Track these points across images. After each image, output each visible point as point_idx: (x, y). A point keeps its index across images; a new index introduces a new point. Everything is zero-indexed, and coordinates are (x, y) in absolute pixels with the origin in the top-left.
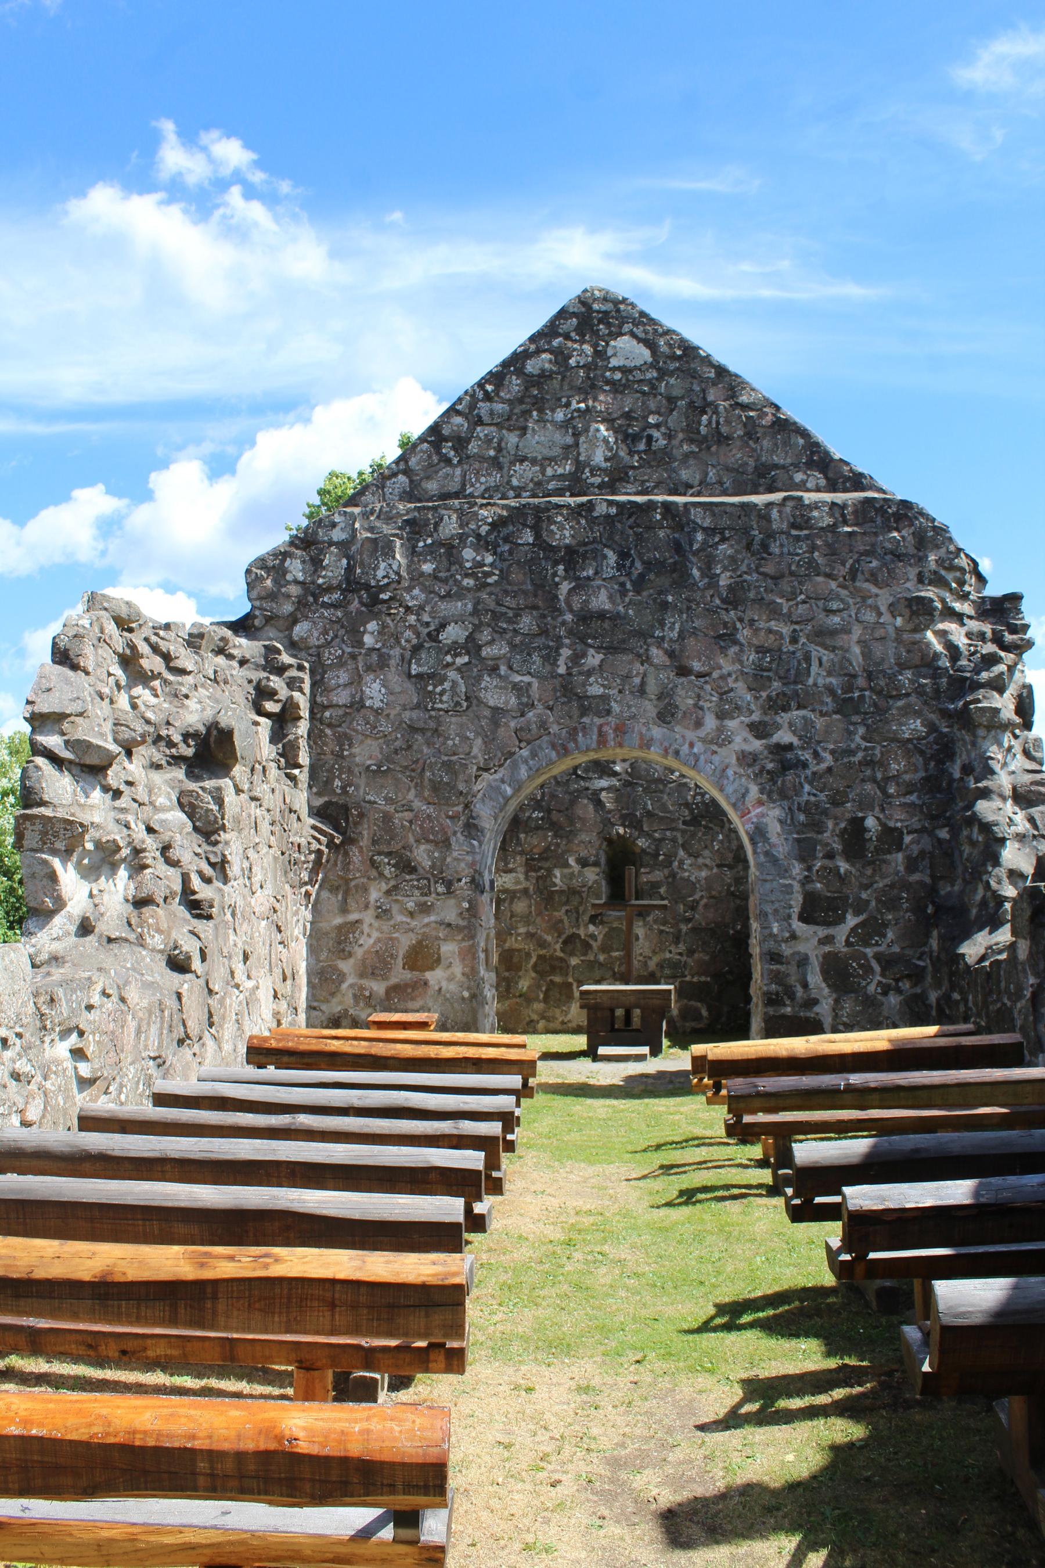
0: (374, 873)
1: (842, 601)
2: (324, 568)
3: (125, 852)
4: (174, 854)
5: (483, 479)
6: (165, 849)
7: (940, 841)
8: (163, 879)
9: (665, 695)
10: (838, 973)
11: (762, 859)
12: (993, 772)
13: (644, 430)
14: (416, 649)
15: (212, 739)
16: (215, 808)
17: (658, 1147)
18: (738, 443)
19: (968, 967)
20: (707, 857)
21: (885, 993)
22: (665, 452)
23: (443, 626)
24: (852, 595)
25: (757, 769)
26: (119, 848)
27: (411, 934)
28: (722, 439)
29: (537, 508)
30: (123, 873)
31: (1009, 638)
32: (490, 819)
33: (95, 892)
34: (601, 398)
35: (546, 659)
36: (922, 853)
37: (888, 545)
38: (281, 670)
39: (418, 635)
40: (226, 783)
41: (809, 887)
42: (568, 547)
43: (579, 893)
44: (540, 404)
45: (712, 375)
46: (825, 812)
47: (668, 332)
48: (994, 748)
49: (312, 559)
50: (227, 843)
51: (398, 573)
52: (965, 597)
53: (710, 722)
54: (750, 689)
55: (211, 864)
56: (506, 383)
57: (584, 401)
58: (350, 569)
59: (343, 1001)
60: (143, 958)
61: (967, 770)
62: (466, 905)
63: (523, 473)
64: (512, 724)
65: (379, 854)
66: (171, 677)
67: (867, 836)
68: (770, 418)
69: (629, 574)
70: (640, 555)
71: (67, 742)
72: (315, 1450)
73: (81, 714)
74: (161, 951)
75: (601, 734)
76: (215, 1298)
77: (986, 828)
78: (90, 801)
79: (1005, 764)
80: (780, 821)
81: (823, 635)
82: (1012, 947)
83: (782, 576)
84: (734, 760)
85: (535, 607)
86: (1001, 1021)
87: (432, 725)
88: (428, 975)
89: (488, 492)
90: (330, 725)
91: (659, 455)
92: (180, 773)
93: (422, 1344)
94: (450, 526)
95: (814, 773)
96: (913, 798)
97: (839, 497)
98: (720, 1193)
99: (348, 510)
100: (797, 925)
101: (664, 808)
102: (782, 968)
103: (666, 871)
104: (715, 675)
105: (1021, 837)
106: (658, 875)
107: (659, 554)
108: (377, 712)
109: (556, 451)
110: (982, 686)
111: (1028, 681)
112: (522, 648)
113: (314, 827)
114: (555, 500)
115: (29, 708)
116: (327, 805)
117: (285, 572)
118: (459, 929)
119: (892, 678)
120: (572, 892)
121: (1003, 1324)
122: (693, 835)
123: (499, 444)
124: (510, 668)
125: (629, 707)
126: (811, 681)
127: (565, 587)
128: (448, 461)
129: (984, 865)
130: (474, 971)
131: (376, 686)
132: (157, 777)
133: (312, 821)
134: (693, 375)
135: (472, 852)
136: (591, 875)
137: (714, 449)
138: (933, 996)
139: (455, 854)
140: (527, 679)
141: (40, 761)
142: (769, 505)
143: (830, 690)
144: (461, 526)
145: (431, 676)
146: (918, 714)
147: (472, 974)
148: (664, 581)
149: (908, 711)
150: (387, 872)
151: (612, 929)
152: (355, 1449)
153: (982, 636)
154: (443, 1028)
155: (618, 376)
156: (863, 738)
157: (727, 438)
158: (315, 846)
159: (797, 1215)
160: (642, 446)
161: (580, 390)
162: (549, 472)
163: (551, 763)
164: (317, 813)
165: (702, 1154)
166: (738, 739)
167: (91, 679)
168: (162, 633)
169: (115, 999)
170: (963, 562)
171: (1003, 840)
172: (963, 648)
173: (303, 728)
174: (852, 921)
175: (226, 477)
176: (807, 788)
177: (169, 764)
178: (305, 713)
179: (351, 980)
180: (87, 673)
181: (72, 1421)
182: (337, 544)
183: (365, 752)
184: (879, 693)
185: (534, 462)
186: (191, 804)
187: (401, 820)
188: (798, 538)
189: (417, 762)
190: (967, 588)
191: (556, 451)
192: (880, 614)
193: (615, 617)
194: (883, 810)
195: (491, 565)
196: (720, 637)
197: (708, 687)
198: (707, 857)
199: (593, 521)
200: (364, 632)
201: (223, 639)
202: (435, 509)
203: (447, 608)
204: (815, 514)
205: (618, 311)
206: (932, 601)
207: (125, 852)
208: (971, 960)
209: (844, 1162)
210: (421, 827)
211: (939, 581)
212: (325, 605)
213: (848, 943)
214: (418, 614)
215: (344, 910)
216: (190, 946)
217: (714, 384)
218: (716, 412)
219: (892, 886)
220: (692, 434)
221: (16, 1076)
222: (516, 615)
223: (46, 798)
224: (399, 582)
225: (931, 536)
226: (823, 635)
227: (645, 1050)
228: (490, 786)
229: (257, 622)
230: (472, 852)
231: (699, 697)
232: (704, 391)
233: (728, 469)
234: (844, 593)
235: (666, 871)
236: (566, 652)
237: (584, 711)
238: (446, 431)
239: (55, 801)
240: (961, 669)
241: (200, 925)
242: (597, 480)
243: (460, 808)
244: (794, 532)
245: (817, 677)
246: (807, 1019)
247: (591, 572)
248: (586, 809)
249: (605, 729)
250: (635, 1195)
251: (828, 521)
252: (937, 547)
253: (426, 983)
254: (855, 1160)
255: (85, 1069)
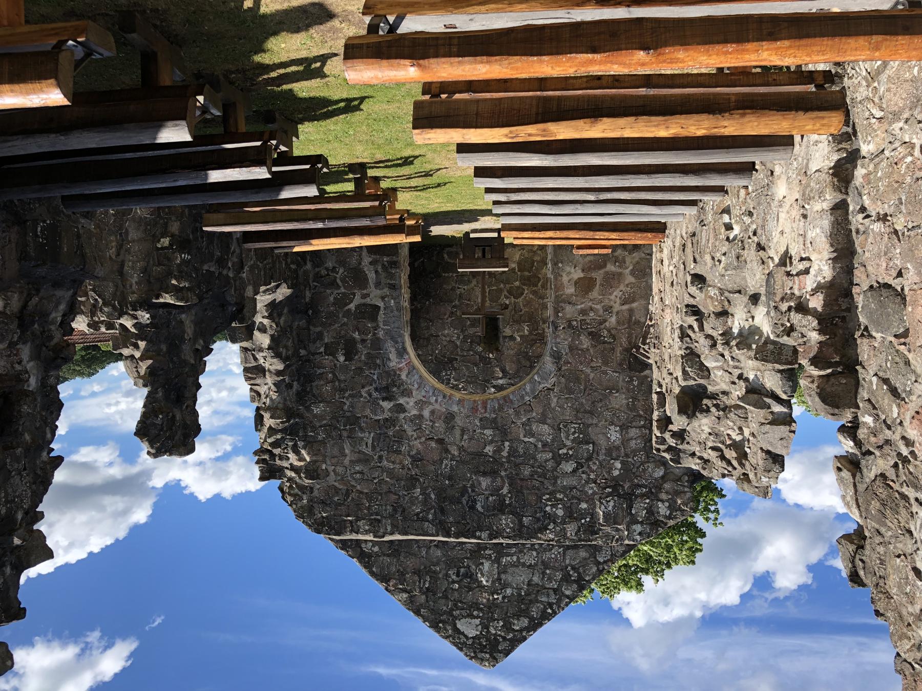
0: (613, 332)
1: (354, 479)
2: (645, 508)
3: (733, 343)
4: (708, 342)
5: (553, 556)
6: (714, 346)
7: (305, 348)
8: (713, 327)
9: (450, 429)
10: (359, 279)
11: (399, 340)
12: (274, 384)
13: (461, 580)
14: (589, 459)
15: (691, 408)
16: (687, 369)
17: (439, 185)
18: (409, 570)
19: (285, 282)
20: (444, 340)
21: (334, 268)
22: (449, 567)
23: (574, 471)
24: (349, 481)
25: (402, 388)
26: (736, 345)
27: (591, 297)
28: (417, 572)
29: (521, 538)
30: (736, 331)
31: (266, 457)
32: (548, 363)
33: (750, 320)
34: (485, 601)
35: (516, 451)
36: (314, 343)
37: (328, 509)
38: (670, 449)
39: (589, 467)
40: (683, 384)
41: (374, 325)
42: (504, 514)
43: (514, 321)
44: (520, 599)
45: (422, 610)
46: (366, 364)
47: (446, 638)
48: (274, 397)
49: (653, 514)
50: (680, 348)
51: (601, 503)
52: (290, 479)
53: (426, 413)
54: (405, 431)
55: (690, 337)
56: (540, 613)
57: (495, 599)
58: (630, 507)
59: (631, 260)
60: (719, 282)
61: (289, 386)
62: (560, 314)
63: (530, 558)
64: (534, 414)
65: (610, 343)
66: (720, 445)
67: (343, 351)
68: (391, 584)
69: (470, 497)
70: (463, 507)
71: (769, 407)
72: (403, 62)
73: (763, 424)
74: (710, 286)
75: (485, 408)
76: (537, 114)
77: (277, 355)
78: (754, 373)
79: (269, 389)
80: (390, 360)
81: (365, 460)
82: (257, 293)
83: (386, 493)
84: (414, 393)
85: (522, 480)
86: (263, 254)
87: (580, 415)
88: (582, 275)
89: (550, 548)
90: (641, 416)
91: (453, 565)
92: (710, 389)
93: (444, 96)
94: (571, 529)
95: (371, 385)
96: (319, 371)
97: (354, 537)
98: (389, 164)
99: (632, 543)
100: (381, 304)
101: (468, 368)
102: (389, 281)
103: (466, 333)
104: (423, 439)
105: (261, 350)
106: (471, 331)
107: (453, 507)
108: (612, 423)
109: (510, 570)
110: (280, 431)
111: (258, 433)
112: (530, 457)
113: (648, 358)
114: (511, 542)
115: (793, 429)
116: (642, 370)
117: (669, 507)
118: (564, 301)
119: (329, 436)
120: (518, 322)
121: (159, 122)
122: (452, 353)
123: (544, 577)
124: (536, 446)
125: (470, 422)
126: (372, 435)
127: (505, 491)
128: (573, 568)
129: (279, 336)
130: (556, 279)
131: (613, 438)
132: (724, 387)
133: (650, 361)
134: (432, 611)
135: (557, 344)
136: (507, 331)
137: (422, 567)
138: (309, 266)
139: (566, 342)
140: (526, 439)
141: (784, 397)
142: (392, 534)
143: (362, 430)
144: (565, 529)
145: (581, 443)
146: (315, 416)
147: (557, 275)
148: (450, 492)
149: (320, 417)
150: (606, 332)
151: (496, 301)
152: (385, 62)
153: (281, 458)
154: (572, 246)
155: (475, 613)
156: (345, 404)
157: (415, 573)
158: (646, 347)
159: (320, 158)
160: (462, 570)
161: (497, 606)
162: (515, 558)
163: (513, 393)
164: (648, 366)
165: (413, 183)
166: (411, 404)
167: (759, 445)
168: (726, 472)
169: (716, 259)
170: (289, 499)
171: (268, 349)
172: (290, 451)
173: (656, 415)
174: (352, 306)
175: (758, 575)
176: (375, 377)
177: (717, 395)
178: (655, 424)
179: (627, 271)
180: (761, 448)
181: (519, 64)
182: (637, 522)
183: (619, 400)
184: (336, 428)
185: (524, 565)
186: (702, 371)
187: (597, 362)
188: (377, 514)
189: (589, 394)
190: (288, 484)
191: (510, 570)
192: (334, 471)
193: (477, 472)
194: (335, 365)
195: (547, 505)
196: (421, 460)
197: (427, 432)
198: (444, 340)
199: (489, 528)
200: (620, 470)
201: (704, 469)
202: (580, 540)
203: (572, 481)
204: (367, 528)
205: (475, 652)
206: (306, 478)
207: (733, 343)
208: (284, 285)
209: (292, 187)
210: (586, 358)
211: (302, 488)
212: (645, 487)
213: (354, 295)
214: (589, 478)
215: (631, 311)
216: (693, 290)
217: (421, 605)
218: (421, 588)
219: (331, 325)
220: (434, 576)
221: (750, 214)
222: (532, 475)
223: (779, 375)
224: (600, 498)
225: (304, 513)
226: (365, 460)
227: (472, 236)
228: (547, 380)
229: (686, 478)
230: (557, 344)
231: (432, 427)
232: (427, 601)
233: (415, 555)
234: (353, 483)
235: (466, 333)
236: (505, 454)
237: (494, 420)
238: (575, 586)
239: (773, 373)
240: (291, 440)
241: (691, 301)
242: (488, 552)
243: (563, 368)
244: (379, 517)
245: (369, 437)
246: (375, 254)
247: (490, 499)
248: (510, 367)
249: (483, 411)
250: (438, 160)
251: (361, 523)
252: (302, 507)
253: (583, 271)
254: (287, 187)
255: (726, 218)
